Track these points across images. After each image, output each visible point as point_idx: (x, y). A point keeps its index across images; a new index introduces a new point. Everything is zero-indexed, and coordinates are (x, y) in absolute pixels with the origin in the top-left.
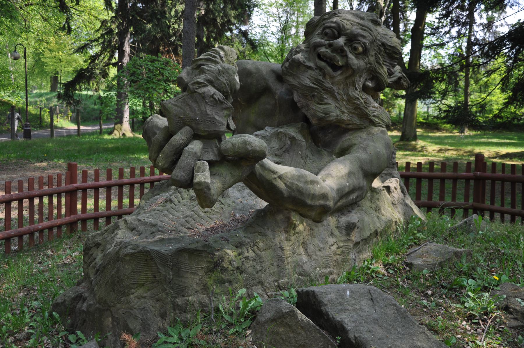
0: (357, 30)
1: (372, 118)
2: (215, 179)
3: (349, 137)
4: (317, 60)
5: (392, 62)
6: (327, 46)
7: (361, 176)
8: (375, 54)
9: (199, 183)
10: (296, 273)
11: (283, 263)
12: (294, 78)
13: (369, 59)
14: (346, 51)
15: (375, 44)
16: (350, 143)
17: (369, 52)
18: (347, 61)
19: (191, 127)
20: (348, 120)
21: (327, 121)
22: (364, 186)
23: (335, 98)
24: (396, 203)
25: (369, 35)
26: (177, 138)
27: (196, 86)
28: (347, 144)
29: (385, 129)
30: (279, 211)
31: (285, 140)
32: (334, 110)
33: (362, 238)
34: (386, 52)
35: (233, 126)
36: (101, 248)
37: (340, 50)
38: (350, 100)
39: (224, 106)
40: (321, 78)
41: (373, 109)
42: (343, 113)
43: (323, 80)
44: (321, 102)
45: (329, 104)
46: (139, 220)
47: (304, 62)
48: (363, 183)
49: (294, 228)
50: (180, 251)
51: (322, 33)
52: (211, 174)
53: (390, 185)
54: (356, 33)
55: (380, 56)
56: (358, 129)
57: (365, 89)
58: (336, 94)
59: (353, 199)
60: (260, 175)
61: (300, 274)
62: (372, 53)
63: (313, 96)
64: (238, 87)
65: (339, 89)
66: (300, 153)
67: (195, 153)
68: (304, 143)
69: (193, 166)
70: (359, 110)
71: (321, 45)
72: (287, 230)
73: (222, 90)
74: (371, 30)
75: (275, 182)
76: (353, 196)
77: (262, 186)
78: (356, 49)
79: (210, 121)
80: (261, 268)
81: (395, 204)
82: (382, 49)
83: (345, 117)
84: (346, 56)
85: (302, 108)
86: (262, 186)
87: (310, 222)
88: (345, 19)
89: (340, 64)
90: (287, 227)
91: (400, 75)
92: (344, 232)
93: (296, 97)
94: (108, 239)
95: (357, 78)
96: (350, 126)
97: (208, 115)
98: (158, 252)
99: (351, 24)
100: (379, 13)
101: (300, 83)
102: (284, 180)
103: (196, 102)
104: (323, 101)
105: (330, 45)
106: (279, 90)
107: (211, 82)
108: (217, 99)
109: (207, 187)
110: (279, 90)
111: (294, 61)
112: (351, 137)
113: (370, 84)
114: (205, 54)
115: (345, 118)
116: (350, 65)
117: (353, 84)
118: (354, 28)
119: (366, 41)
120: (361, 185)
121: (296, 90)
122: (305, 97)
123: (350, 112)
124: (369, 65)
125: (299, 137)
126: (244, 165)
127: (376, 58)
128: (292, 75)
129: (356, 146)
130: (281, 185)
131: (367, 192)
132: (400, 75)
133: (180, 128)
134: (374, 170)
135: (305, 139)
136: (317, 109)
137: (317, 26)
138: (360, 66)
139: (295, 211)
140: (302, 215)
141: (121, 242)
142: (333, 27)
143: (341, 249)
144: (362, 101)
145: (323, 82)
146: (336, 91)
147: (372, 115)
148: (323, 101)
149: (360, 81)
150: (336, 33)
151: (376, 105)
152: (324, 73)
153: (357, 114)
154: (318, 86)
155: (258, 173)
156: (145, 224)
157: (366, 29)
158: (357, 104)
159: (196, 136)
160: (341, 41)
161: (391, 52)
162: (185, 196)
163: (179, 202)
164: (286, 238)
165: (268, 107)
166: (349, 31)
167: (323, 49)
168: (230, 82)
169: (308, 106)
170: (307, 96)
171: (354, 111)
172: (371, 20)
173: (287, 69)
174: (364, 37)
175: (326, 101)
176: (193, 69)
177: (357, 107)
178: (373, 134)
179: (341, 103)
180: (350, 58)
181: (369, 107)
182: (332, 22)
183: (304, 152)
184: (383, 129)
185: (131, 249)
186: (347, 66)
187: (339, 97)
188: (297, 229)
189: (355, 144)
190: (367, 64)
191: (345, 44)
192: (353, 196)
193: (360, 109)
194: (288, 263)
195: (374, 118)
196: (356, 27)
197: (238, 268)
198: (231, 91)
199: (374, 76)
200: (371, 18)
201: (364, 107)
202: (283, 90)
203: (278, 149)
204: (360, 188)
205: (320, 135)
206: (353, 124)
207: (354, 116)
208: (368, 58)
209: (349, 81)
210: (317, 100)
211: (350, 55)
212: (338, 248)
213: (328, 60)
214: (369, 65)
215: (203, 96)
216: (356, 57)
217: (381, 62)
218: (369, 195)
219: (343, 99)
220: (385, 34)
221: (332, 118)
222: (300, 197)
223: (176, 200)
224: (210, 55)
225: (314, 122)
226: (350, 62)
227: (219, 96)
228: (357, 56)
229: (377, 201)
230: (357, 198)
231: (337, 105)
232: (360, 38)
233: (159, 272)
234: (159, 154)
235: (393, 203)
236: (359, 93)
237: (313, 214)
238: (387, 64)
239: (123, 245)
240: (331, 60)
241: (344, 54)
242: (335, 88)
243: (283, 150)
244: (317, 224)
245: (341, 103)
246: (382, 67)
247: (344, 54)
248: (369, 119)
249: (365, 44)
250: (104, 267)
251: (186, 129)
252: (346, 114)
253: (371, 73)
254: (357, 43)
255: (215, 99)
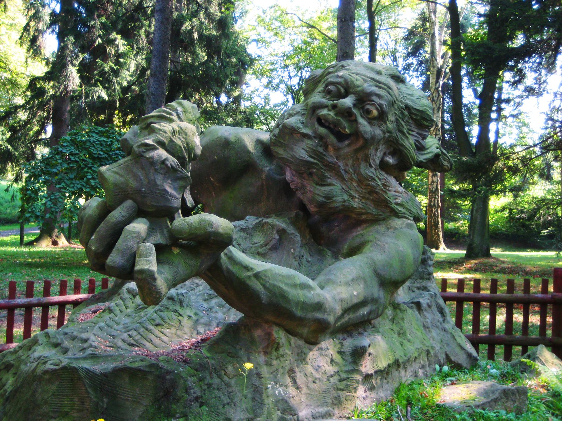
0: (369, 87)
1: (394, 206)
2: (163, 268)
3: (362, 232)
4: (317, 125)
5: (420, 132)
6: (330, 107)
7: (375, 284)
8: (397, 119)
9: (142, 272)
10: (278, 410)
11: (261, 396)
12: (285, 150)
13: (387, 127)
14: (355, 115)
15: (396, 106)
16: (362, 239)
17: (387, 116)
18: (357, 127)
19: (135, 200)
20: (360, 208)
21: (330, 208)
22: (379, 298)
23: (341, 178)
24: (430, 325)
25: (387, 94)
26: (116, 215)
27: (142, 149)
28: (358, 240)
29: (413, 222)
30: (257, 325)
31: (272, 233)
32: (338, 192)
33: (377, 368)
34: (412, 118)
35: (190, 201)
36: (13, 370)
37: (348, 112)
38: (362, 181)
39: (179, 175)
40: (321, 149)
41: (396, 194)
42: (353, 197)
43: (324, 153)
44: (322, 182)
45: (333, 185)
46: (66, 334)
47: (299, 128)
48: (377, 292)
49: (277, 349)
50: (118, 372)
51: (324, 91)
52: (159, 262)
53: (421, 300)
54: (369, 91)
55: (402, 122)
56: (375, 221)
57: (384, 166)
58: (343, 172)
59: (364, 314)
60: (228, 271)
61: (284, 411)
62: (392, 118)
63: (311, 174)
64: (199, 151)
65: (347, 165)
66: (292, 251)
67: (138, 233)
68: (299, 238)
69: (135, 249)
70: (375, 195)
71: (322, 106)
72: (268, 350)
73: (176, 155)
74: (390, 88)
75: (248, 282)
76: (365, 311)
77: (231, 286)
78: (368, 112)
79: (159, 193)
80: (229, 401)
81: (428, 328)
82: (406, 113)
83: (356, 204)
84: (356, 121)
85: (297, 190)
86: (231, 286)
87: (301, 342)
88: (357, 74)
89: (347, 131)
90: (267, 347)
91: (438, 150)
92: (349, 358)
93: (288, 176)
94: (23, 357)
95: (372, 151)
96: (364, 217)
97: (157, 185)
98: (87, 371)
99: (363, 79)
100: (435, 73)
101: (293, 157)
102: (262, 279)
103: (143, 168)
104: (324, 181)
105: (334, 107)
106: (267, 167)
107: (161, 144)
108: (170, 165)
109: (151, 276)
110: (267, 167)
111: (285, 126)
112: (364, 231)
113: (390, 160)
114: (157, 110)
115: (355, 205)
116: (361, 133)
117: (367, 159)
118: (366, 85)
119: (382, 102)
120: (376, 296)
121: (289, 166)
122: (300, 174)
123: (363, 198)
124: (387, 134)
125: (291, 230)
126: (203, 253)
127: (397, 125)
128: (282, 145)
129: (371, 244)
130: (257, 286)
131: (385, 307)
132: (438, 150)
133: (121, 202)
134: (395, 274)
135: (300, 232)
136: (317, 192)
137: (320, 82)
138: (375, 134)
139: (278, 325)
140: (290, 332)
141: (39, 358)
142: (339, 83)
143: (345, 382)
144: (379, 183)
145: (324, 155)
146: (342, 167)
147: (393, 201)
148: (324, 181)
149: (376, 155)
150: (342, 90)
151: (401, 189)
152: (326, 143)
153: (373, 201)
154: (318, 161)
155: (224, 267)
156: (74, 338)
157: (386, 87)
158: (372, 186)
159: (139, 213)
160: (348, 101)
161: (418, 118)
162: (130, 304)
163: (121, 311)
164: (266, 361)
165: (251, 189)
166: (360, 88)
167: (325, 112)
168: (187, 144)
169: (303, 187)
170: (302, 174)
171: (367, 196)
172: (390, 75)
173: (276, 137)
174: (380, 96)
175: (329, 181)
176: (142, 129)
177: (372, 191)
178: (395, 229)
179: (349, 184)
180: (360, 124)
181: (389, 191)
182: (338, 76)
183: (298, 250)
184: (409, 222)
185: (52, 364)
186: (357, 134)
187: (346, 176)
188: (281, 351)
189: (370, 241)
190: (384, 133)
191: (354, 105)
192: (365, 311)
193: (377, 193)
194: (268, 396)
195: (396, 207)
196: (370, 83)
197: (197, 399)
198: (189, 157)
199: (396, 148)
200: (391, 72)
201: (382, 190)
202: (273, 167)
203: (262, 246)
204: (375, 301)
205: (324, 229)
206: (367, 213)
207: (369, 202)
208: (386, 124)
209: (360, 155)
210: (316, 178)
211: (361, 121)
212: (340, 380)
213: (332, 126)
214: (387, 134)
215: (152, 162)
216: (369, 123)
217: (405, 131)
218: (389, 312)
219: (352, 179)
220: (409, 95)
221: (336, 205)
222: (284, 305)
223: (117, 309)
224: (164, 111)
225: (312, 209)
226: (361, 128)
227: (172, 161)
228: (371, 121)
229: (401, 321)
230: (370, 313)
231: (344, 187)
232: (374, 98)
233: (89, 397)
234: (92, 236)
235: (424, 326)
236: (374, 171)
237: (305, 331)
238: (415, 134)
239: (43, 360)
240: (335, 126)
241: (353, 118)
242: (341, 164)
243: (269, 247)
244: (311, 346)
245: (349, 184)
246: (407, 138)
247: (353, 118)
248: (389, 207)
249: (380, 105)
250: (16, 391)
251: (128, 203)
252: (357, 200)
253: (391, 145)
254: (371, 105)
255: (167, 166)
